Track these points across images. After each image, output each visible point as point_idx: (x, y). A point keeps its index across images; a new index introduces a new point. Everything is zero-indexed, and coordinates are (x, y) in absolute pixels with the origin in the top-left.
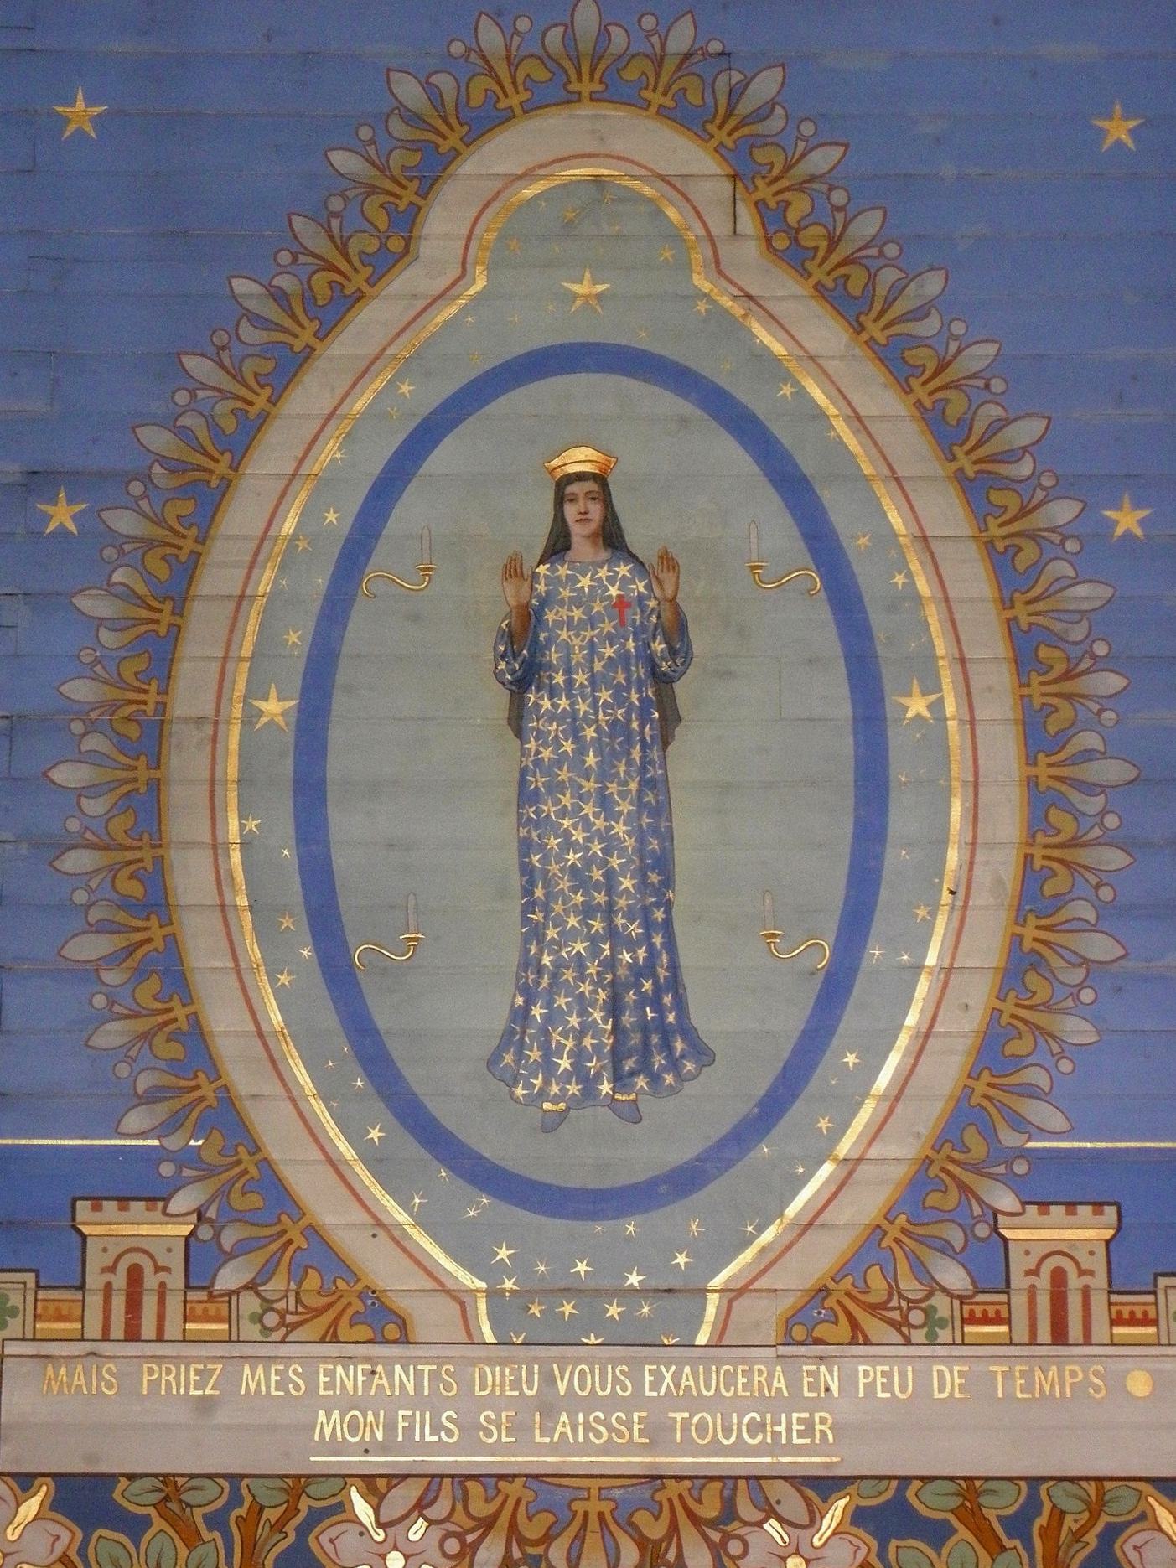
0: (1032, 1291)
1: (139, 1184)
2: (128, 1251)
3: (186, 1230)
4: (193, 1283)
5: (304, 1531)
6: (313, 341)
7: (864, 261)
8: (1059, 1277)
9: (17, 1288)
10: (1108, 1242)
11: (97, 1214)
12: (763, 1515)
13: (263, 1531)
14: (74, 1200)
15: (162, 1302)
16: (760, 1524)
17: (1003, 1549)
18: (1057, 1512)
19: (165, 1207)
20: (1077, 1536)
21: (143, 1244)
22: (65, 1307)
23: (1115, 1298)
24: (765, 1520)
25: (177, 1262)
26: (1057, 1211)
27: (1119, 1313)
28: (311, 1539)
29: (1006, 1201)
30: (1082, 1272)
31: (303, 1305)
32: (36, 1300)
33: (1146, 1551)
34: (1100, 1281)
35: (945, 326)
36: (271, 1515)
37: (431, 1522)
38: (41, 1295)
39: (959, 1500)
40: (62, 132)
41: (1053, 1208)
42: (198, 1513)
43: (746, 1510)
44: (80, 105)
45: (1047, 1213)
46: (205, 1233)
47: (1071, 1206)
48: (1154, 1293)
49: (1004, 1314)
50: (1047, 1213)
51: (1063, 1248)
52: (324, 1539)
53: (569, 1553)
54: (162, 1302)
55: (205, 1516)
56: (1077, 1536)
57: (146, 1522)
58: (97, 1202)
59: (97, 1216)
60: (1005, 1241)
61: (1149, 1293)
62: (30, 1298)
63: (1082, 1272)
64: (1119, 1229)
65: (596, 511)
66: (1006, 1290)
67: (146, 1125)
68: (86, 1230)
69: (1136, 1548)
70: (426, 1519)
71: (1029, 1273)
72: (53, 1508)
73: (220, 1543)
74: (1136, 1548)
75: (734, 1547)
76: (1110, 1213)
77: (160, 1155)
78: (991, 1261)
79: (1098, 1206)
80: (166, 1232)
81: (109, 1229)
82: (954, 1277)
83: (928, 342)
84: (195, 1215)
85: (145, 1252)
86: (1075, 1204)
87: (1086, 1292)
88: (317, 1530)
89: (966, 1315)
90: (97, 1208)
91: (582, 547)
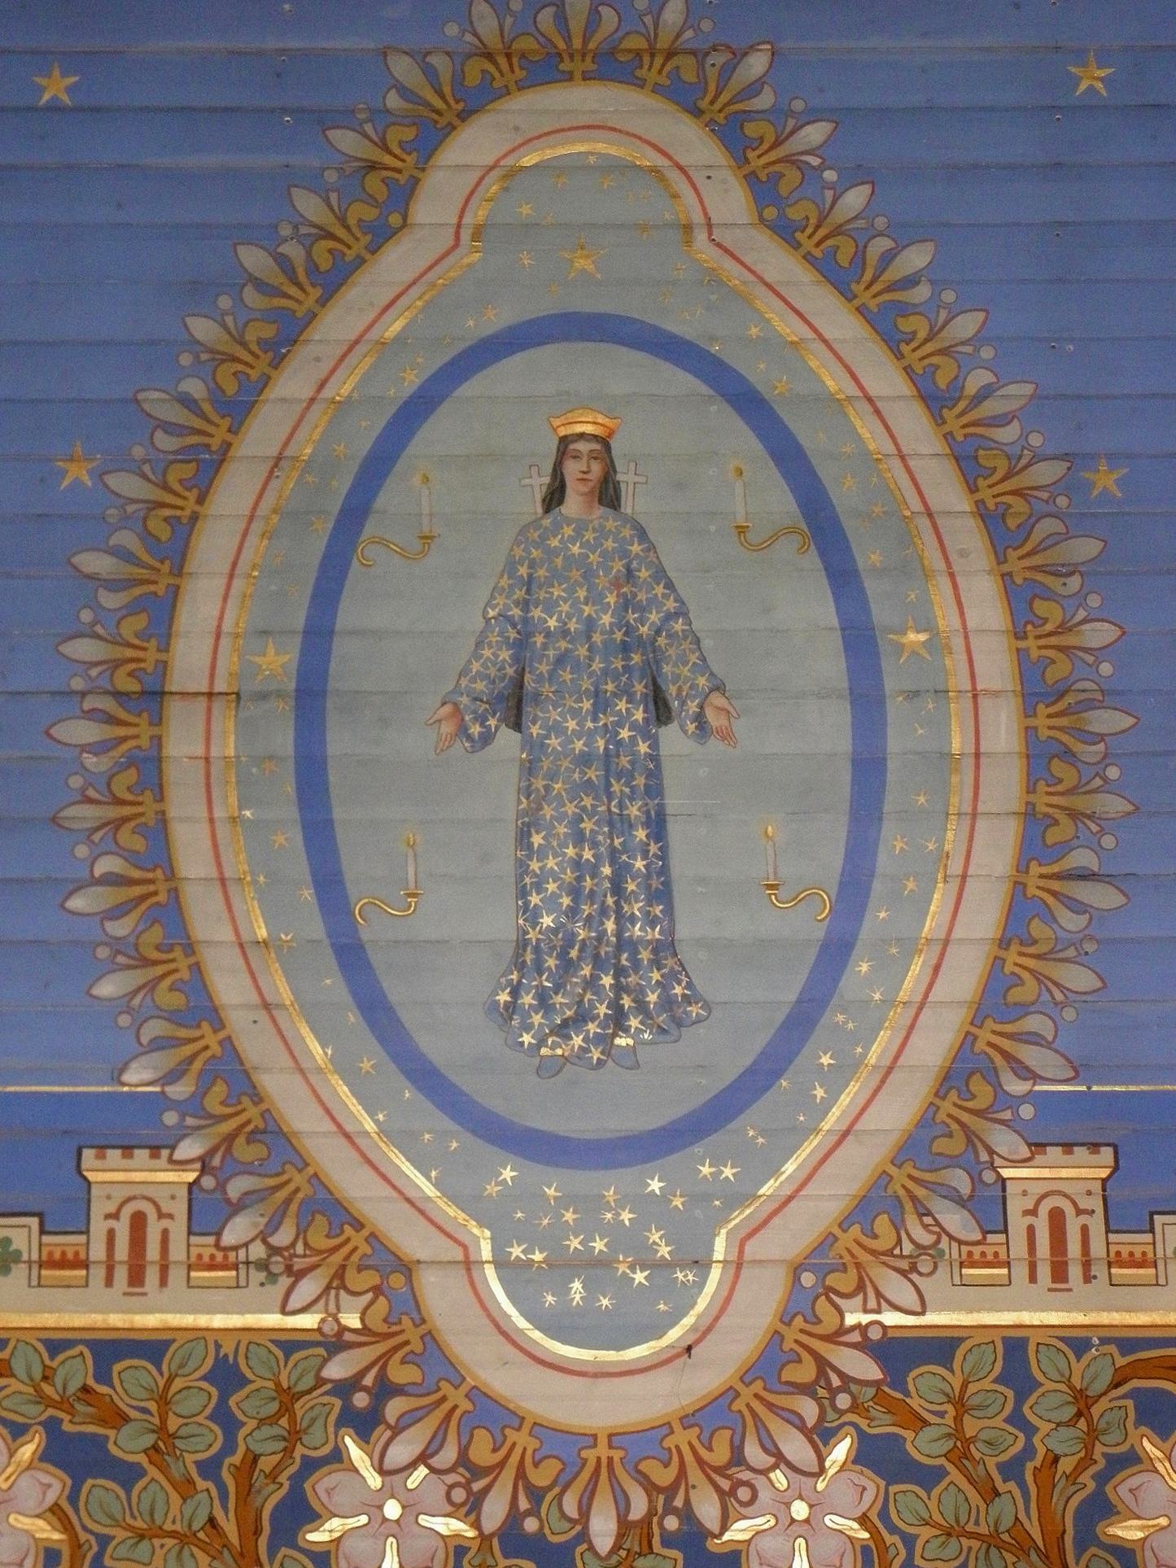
0: (111, 1235)
1: (137, 1129)
3: (191, 1177)
5: (298, 1479)
6: (267, 370)
7: (240, 325)
8: (138, 1221)
9: (22, 1235)
10: (1104, 1181)
11: (129, 1162)
12: (772, 1460)
13: (259, 1480)
16: (764, 1473)
17: (997, 1494)
18: (152, 1452)
19: (171, 1155)
20: (273, 1476)
24: (774, 1467)
25: (180, 1209)
26: (141, 1155)
28: (1108, 1489)
29: (1005, 1141)
31: (311, 1248)
32: (40, 1245)
33: (1141, 1494)
34: (1097, 1225)
35: (936, 295)
36: (1066, 1465)
37: (433, 1470)
38: (46, 1239)
39: (951, 1444)
41: (137, 1152)
42: (991, 1464)
43: (753, 1452)
45: (131, 1156)
46: (208, 1182)
48: (1152, 1231)
49: (1003, 1256)
50: (131, 1156)
51: (150, 1192)
52: (1123, 1491)
53: (580, 1502)
55: (999, 1466)
56: (273, 1476)
57: (136, 1472)
58: (102, 1149)
59: (98, 1164)
60: (1004, 1180)
61: (81, 1233)
64: (1116, 1168)
65: (597, 469)
67: (148, 1075)
68: (90, 1176)
69: (49, 1486)
70: (428, 1466)
71: (108, 1216)
72: (41, 1459)
73: (214, 1493)
74: (49, 1486)
75: (744, 1494)
76: (1107, 1154)
77: (161, 1102)
78: (989, 1206)
80: (167, 1179)
82: (955, 1220)
83: (921, 309)
84: (198, 1165)
85: (1066, 1196)
86: (1045, 1145)
87: (1085, 1230)
90: (101, 1156)
91: (573, 505)
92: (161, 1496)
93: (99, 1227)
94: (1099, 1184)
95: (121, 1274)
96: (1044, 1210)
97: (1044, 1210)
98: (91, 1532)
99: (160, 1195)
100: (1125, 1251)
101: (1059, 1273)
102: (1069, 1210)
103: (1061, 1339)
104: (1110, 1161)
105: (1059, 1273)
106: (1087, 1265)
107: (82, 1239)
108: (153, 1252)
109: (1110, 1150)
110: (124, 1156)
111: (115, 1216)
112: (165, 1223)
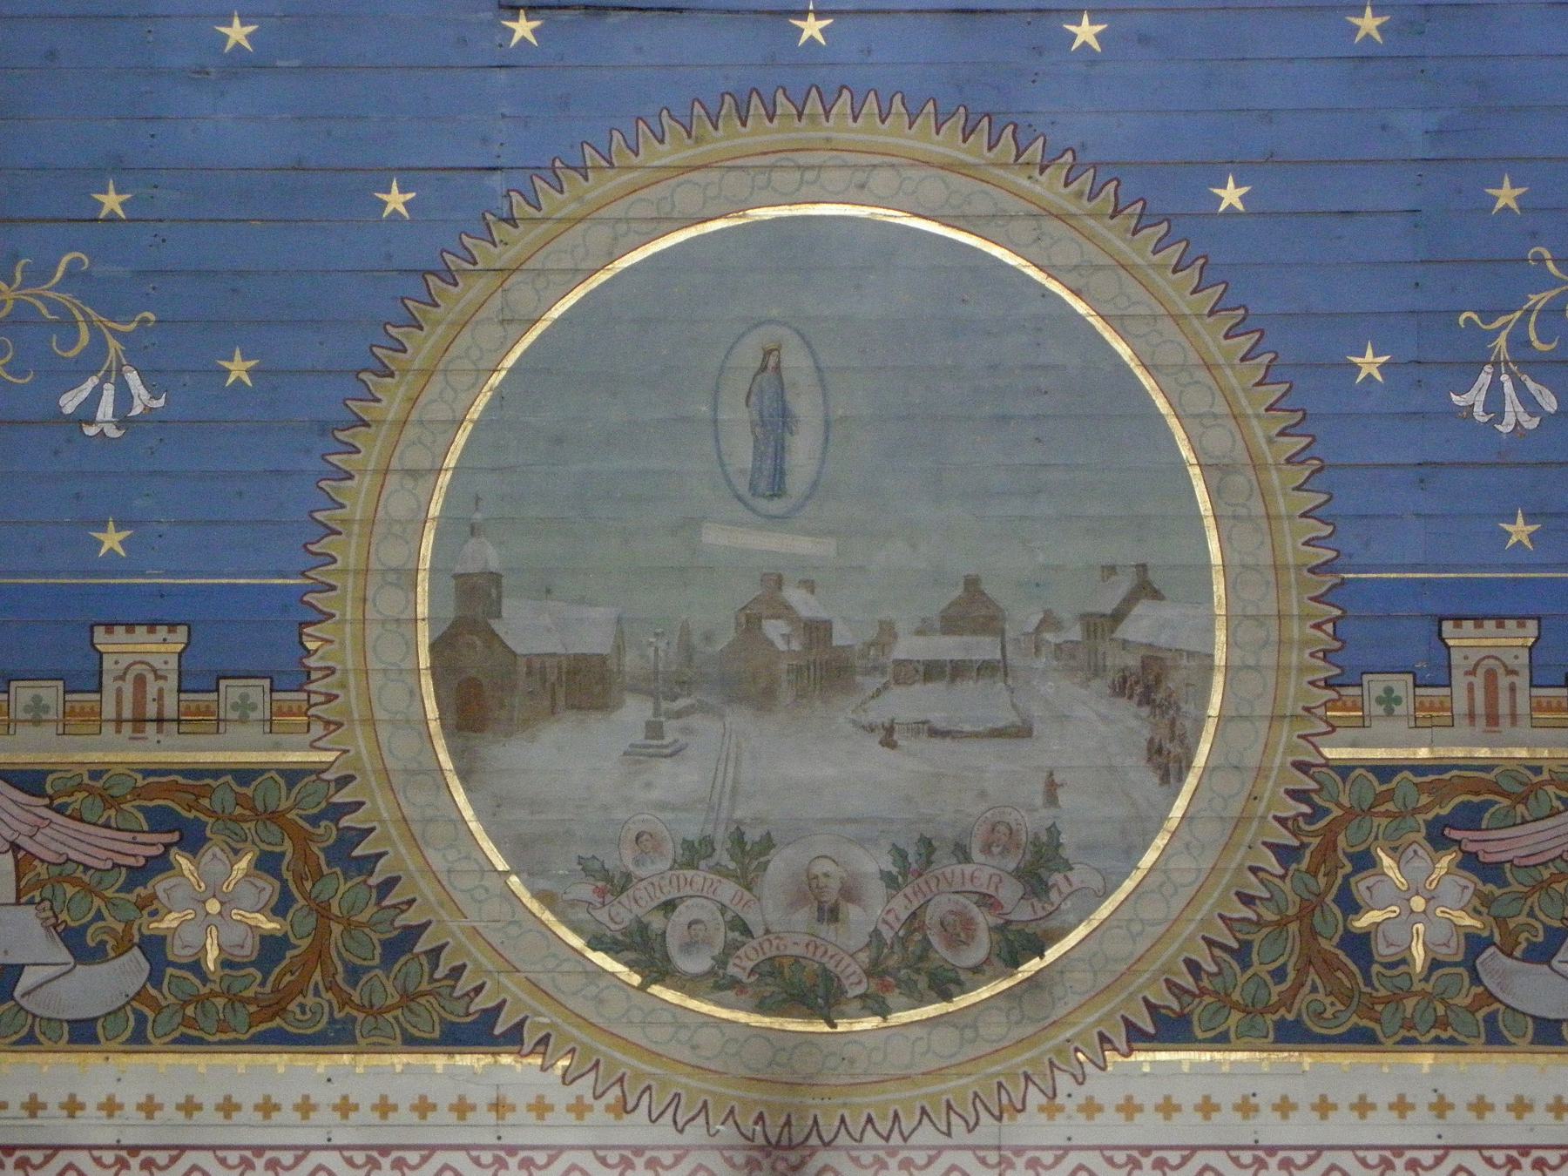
0: (119, 691)
4: (185, 685)
10: (180, 654)
14: (92, 627)
21: (148, 658)
22: (1436, 700)
27: (1539, 703)
30: (158, 677)
34: (1522, 681)
40: (1094, 50)
45: (1481, 626)
47: (1500, 620)
48: (217, 690)
50: (1481, 626)
51: (1493, 652)
58: (109, 626)
59: (109, 638)
60: (101, 654)
62: (267, 699)
63: (158, 677)
64: (187, 645)
66: (99, 690)
68: (1451, 642)
69: (214, 855)
74: (214, 855)
76: (1532, 626)
79: (172, 626)
81: (121, 649)
85: (1496, 658)
90: (1500, 626)
94: (1526, 652)
95: (1481, 722)
97: (130, 677)
100: (193, 706)
102: (1501, 671)
103: (1527, 767)
107: (1446, 691)
109: (1535, 622)
111: (1473, 673)
112: (161, 683)
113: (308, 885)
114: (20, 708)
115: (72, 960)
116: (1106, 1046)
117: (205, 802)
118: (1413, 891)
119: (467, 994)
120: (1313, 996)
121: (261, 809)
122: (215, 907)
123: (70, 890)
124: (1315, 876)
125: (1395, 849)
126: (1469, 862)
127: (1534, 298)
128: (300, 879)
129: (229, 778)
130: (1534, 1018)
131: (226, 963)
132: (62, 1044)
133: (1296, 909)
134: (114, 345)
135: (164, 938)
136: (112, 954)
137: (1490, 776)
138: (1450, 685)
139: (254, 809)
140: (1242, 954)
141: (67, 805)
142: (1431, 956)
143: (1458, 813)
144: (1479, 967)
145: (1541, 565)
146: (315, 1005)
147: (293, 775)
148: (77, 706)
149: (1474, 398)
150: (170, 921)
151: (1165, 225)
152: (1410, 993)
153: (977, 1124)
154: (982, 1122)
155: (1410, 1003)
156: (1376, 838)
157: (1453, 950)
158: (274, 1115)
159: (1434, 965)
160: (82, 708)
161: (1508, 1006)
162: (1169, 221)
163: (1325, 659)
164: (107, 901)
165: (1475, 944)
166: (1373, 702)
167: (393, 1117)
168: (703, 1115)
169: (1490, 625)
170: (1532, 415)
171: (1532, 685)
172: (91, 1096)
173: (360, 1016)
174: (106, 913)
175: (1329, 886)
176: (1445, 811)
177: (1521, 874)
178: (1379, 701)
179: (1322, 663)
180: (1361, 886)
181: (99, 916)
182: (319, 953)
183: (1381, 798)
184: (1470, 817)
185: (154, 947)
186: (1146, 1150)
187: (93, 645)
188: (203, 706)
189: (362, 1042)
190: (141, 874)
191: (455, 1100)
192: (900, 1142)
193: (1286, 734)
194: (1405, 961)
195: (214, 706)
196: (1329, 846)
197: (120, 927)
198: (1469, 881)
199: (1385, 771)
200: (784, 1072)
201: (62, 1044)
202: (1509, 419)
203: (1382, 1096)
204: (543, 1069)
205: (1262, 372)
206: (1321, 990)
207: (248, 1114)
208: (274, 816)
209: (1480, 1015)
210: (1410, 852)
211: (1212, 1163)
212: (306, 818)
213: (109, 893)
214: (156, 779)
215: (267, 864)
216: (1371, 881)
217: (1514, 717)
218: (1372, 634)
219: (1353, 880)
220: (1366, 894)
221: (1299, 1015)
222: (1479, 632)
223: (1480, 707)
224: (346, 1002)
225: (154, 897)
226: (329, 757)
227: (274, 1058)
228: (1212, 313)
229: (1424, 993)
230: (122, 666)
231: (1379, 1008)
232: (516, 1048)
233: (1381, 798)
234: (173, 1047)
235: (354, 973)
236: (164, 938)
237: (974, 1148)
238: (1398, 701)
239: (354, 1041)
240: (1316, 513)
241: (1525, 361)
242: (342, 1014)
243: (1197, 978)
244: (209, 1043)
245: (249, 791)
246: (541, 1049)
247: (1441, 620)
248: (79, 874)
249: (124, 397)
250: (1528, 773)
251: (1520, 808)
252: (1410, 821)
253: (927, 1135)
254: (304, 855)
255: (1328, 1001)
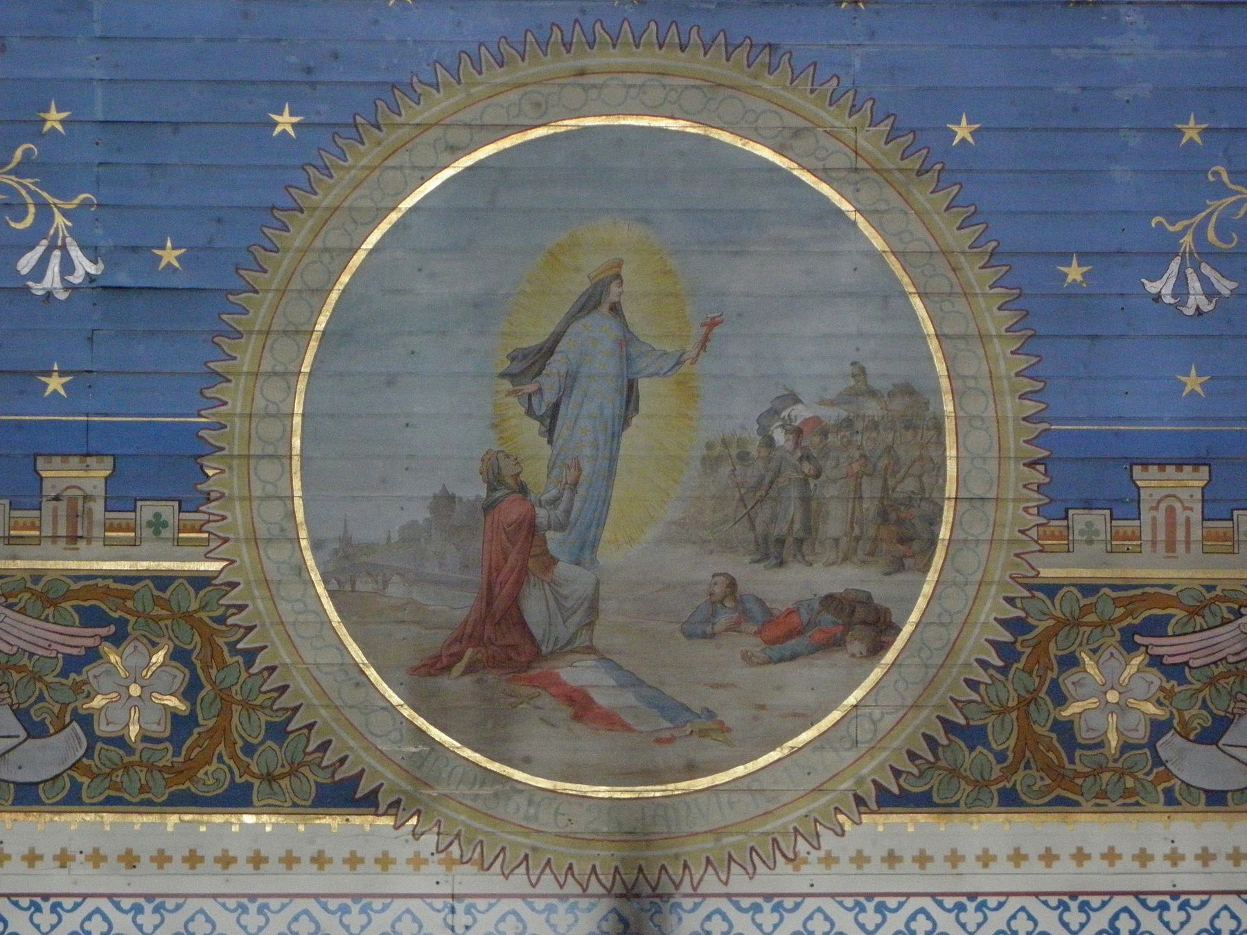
2: (1169, 496)
8: (1171, 511)
10: (1203, 488)
15: (1154, 535)
23: (1207, 524)
27: (16, 523)
34: (1196, 515)
44: (1192, 123)
45: (1147, 470)
49: (37, 523)
50: (1147, 470)
51: (74, 482)
54: (1154, 535)
59: (48, 466)
60: (1139, 488)
63: (1186, 508)
64: (114, 470)
68: (44, 474)
69: (1112, 654)
71: (1152, 508)
74: (1112, 654)
81: (58, 474)
85: (78, 488)
86: (1147, 464)
88: (187, 679)
89: (12, 523)
92: (246, 726)
93: (1146, 515)
95: (1161, 547)
96: (1163, 506)
98: (1151, 770)
99: (1183, 495)
101: (1171, 546)
104: (110, 465)
105: (1171, 546)
106: (1188, 543)
107: (1137, 523)
108: (1180, 534)
110: (1194, 470)
111: (1156, 508)
113: (213, 672)
114: (1076, 532)
115: (23, 734)
116: (862, 809)
117: (129, 604)
118: (1109, 685)
119: (333, 764)
120: (1028, 771)
121: (175, 608)
122: (136, 692)
123: (16, 676)
124: (1030, 674)
125: (1094, 651)
126: (1156, 661)
127: (1215, 204)
128: (206, 667)
129: (148, 582)
130: (1206, 791)
131: (145, 738)
132: (1201, 806)
133: (1015, 703)
134: (60, 220)
135: (1071, 722)
136: (52, 731)
137: (1172, 592)
138: (40, 509)
139: (171, 610)
140: (278, 732)
141: (16, 604)
142: (1123, 738)
143: (1139, 620)
144: (1159, 750)
145: (1149, 419)
146: (212, 777)
147: (200, 581)
148: (1121, 530)
149: (1164, 287)
150: (98, 702)
151: (911, 136)
152: (1107, 769)
153: (754, 873)
154: (758, 871)
155: (1106, 776)
156: (1080, 645)
157: (1141, 734)
158: (929, 865)
159: (1125, 747)
160: (1125, 532)
161: (1183, 782)
162: (914, 132)
163: (1038, 491)
164: (48, 686)
165: (1159, 728)
166: (170, 523)
167: (1151, 866)
168: (524, 865)
169: (1170, 469)
170: (1174, 295)
171: (106, 510)
172: (971, 850)
173: (256, 783)
174: (46, 695)
175: (1041, 685)
176: (1136, 622)
177: (1197, 673)
178: (150, 524)
179: (1036, 495)
180: (1068, 682)
181: (41, 698)
182: (221, 732)
183: (1085, 610)
184: (1156, 627)
185: (86, 721)
186: (1073, 896)
187: (35, 471)
188: (124, 523)
189: (1231, 806)
190: (74, 664)
191: (283, 854)
192: (690, 891)
193: (1002, 555)
194: (1101, 744)
195: (132, 525)
196: (1040, 646)
197: (56, 709)
198: (1155, 678)
199: (1088, 589)
200: (638, 833)
201: (994, 808)
202: (1192, 301)
203: (1065, 849)
204: (396, 827)
205: (987, 258)
206: (1033, 766)
207: (970, 865)
208: (188, 616)
209: (1160, 788)
210: (1106, 655)
211: (518, 909)
212: (212, 619)
213: (49, 679)
214: (87, 583)
215: (179, 656)
216: (1076, 678)
217: (1154, 543)
218: (1083, 475)
219: (1060, 680)
220: (1071, 687)
221: (1014, 785)
222: (1163, 475)
223: (1161, 536)
224: (247, 770)
225: (86, 682)
226: (216, 566)
227: (327, 820)
228: (947, 209)
229: (1114, 770)
230: (1157, 497)
231: (1079, 781)
232: (373, 810)
233: (1085, 610)
234: (1047, 809)
235: (249, 749)
236: (1071, 722)
237: (729, 896)
238: (165, 525)
239: (39, 802)
240: (1025, 373)
241: (1206, 254)
242: (243, 780)
243: (317, 750)
244: (130, 803)
245: (167, 595)
246: (393, 811)
247: (36, 456)
248: (25, 661)
249: (67, 266)
250: (69, 581)
251: (1199, 620)
252: (1108, 631)
253: (548, 883)
254: (215, 651)
255: (1037, 774)
